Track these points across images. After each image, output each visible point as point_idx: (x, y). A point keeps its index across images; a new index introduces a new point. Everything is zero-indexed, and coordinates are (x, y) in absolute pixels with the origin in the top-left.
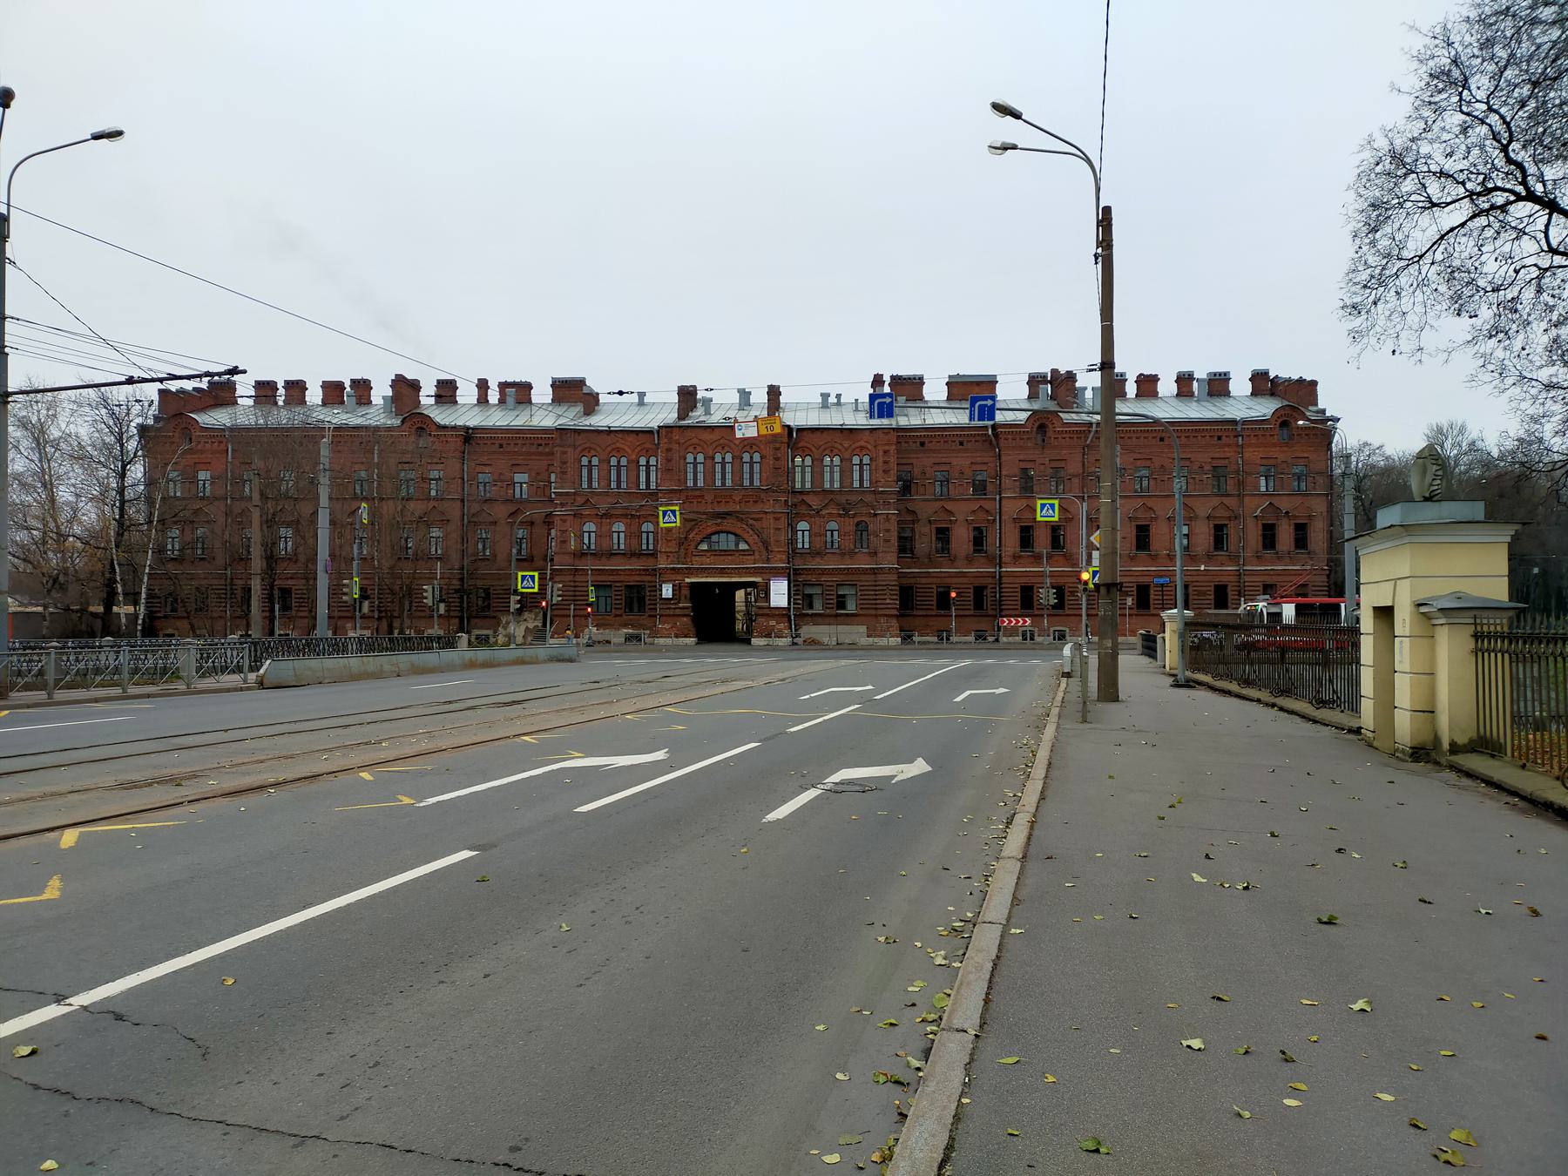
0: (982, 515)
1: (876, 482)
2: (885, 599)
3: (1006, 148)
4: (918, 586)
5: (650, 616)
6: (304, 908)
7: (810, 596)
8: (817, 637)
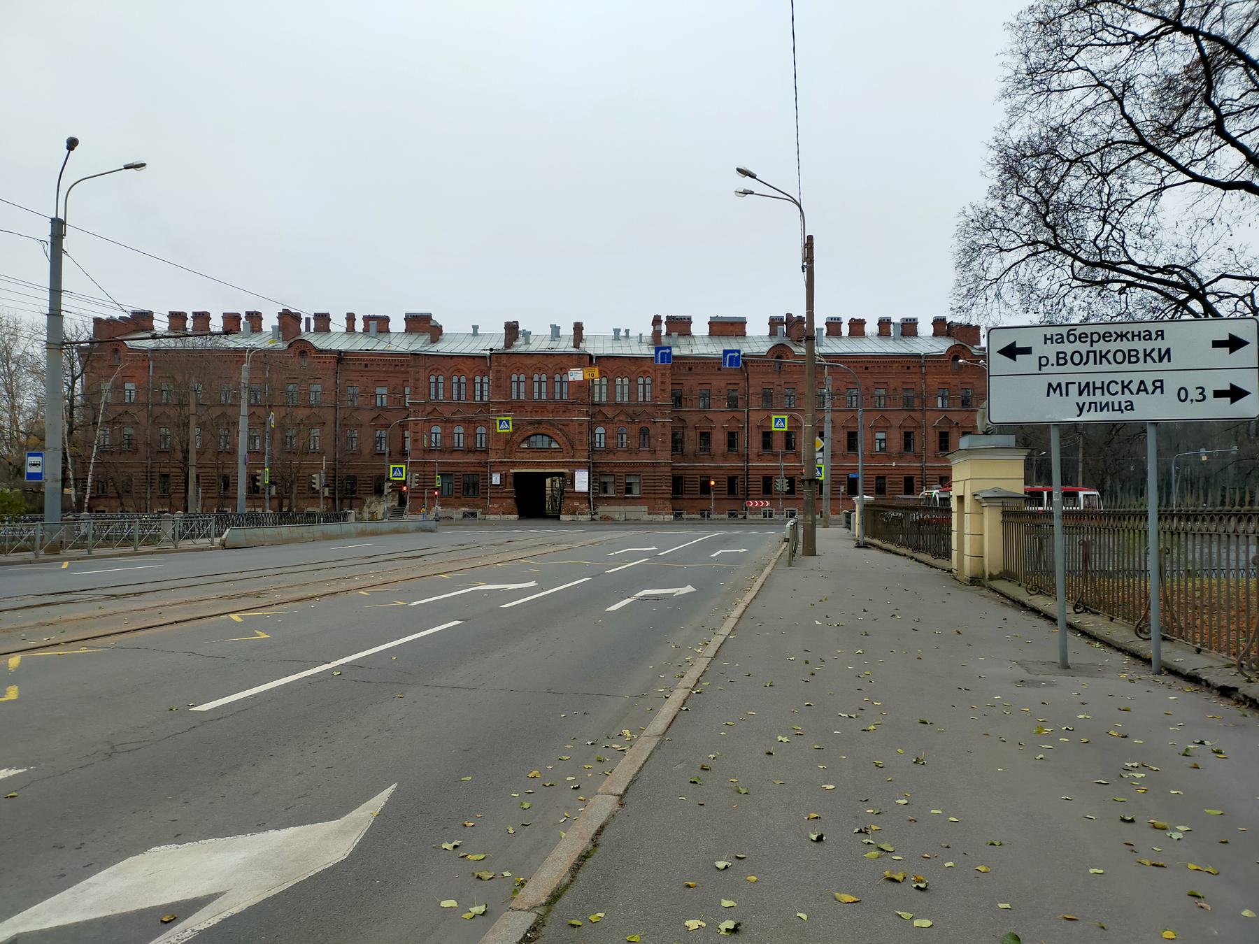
0: (734, 424)
1: (656, 397)
2: (662, 486)
3: (746, 193)
4: (686, 476)
5: (482, 498)
6: (398, 639)
7: (605, 483)
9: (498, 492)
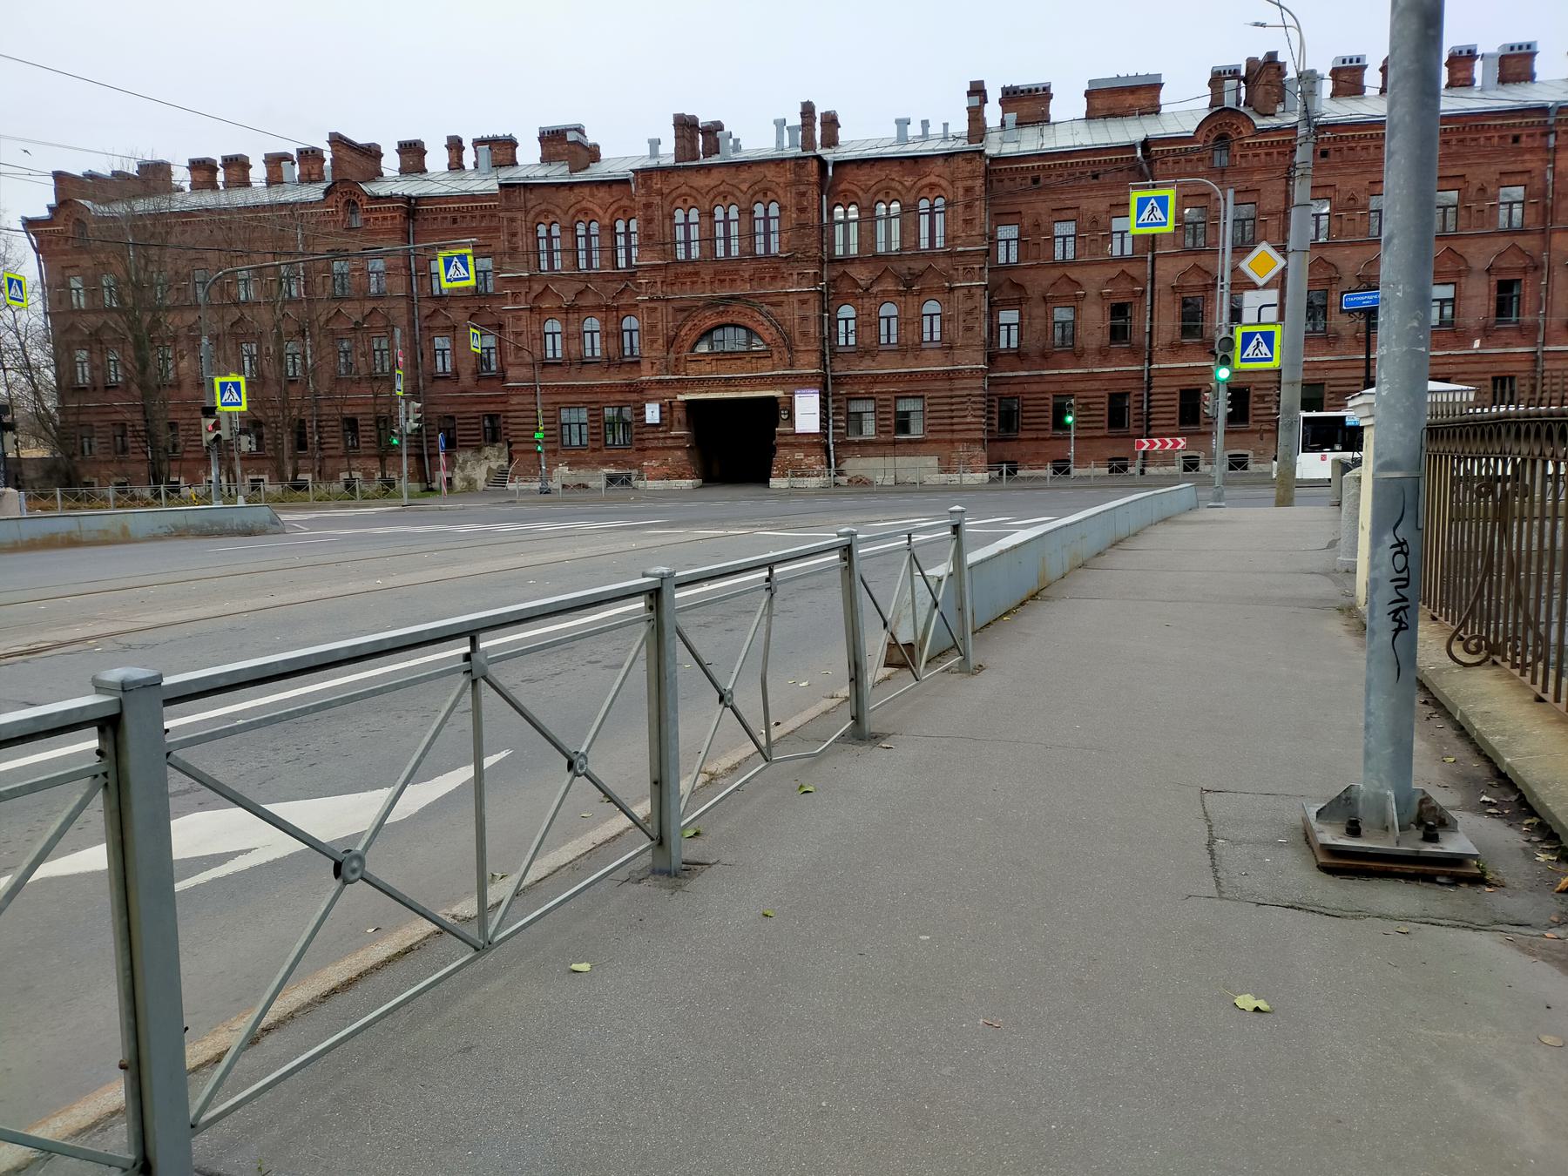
0: (1124, 286)
2: (965, 416)
4: (1026, 396)
5: (638, 450)
8: (868, 475)
9: (658, 438)
